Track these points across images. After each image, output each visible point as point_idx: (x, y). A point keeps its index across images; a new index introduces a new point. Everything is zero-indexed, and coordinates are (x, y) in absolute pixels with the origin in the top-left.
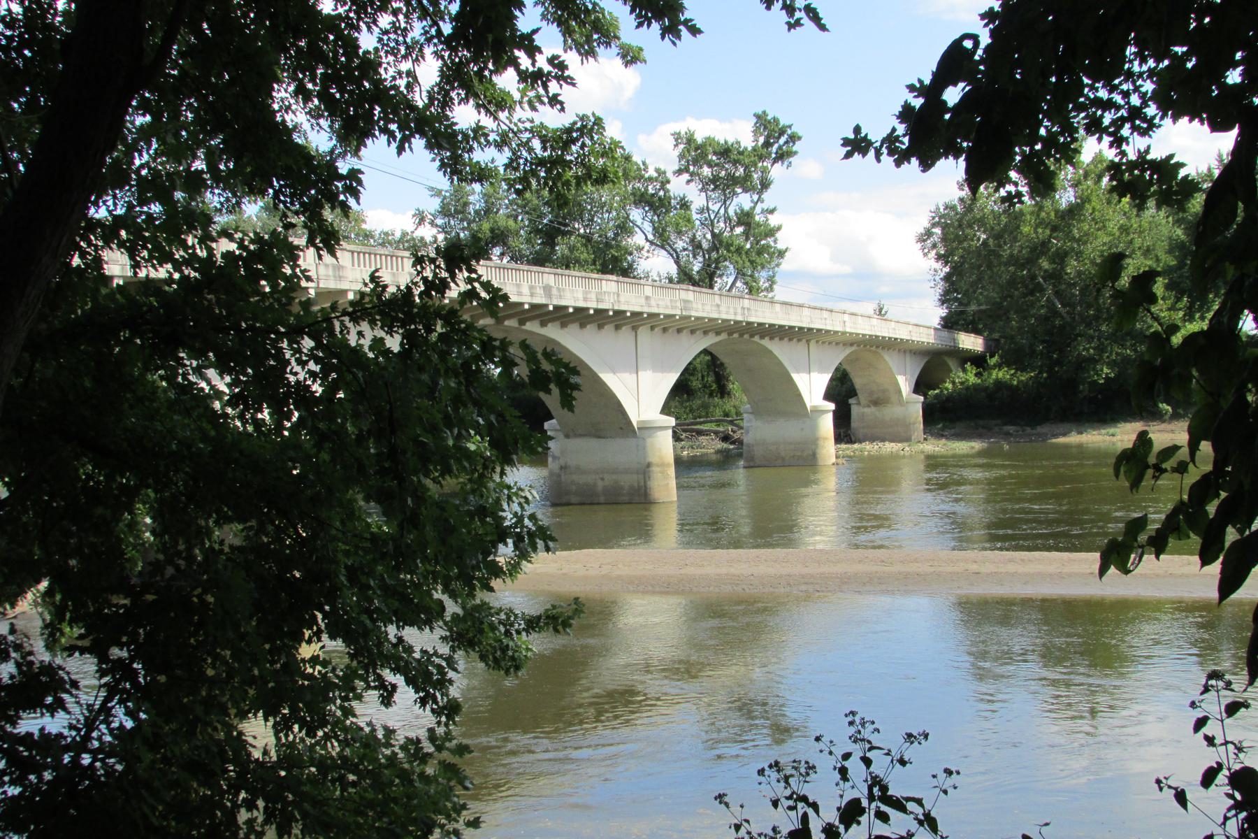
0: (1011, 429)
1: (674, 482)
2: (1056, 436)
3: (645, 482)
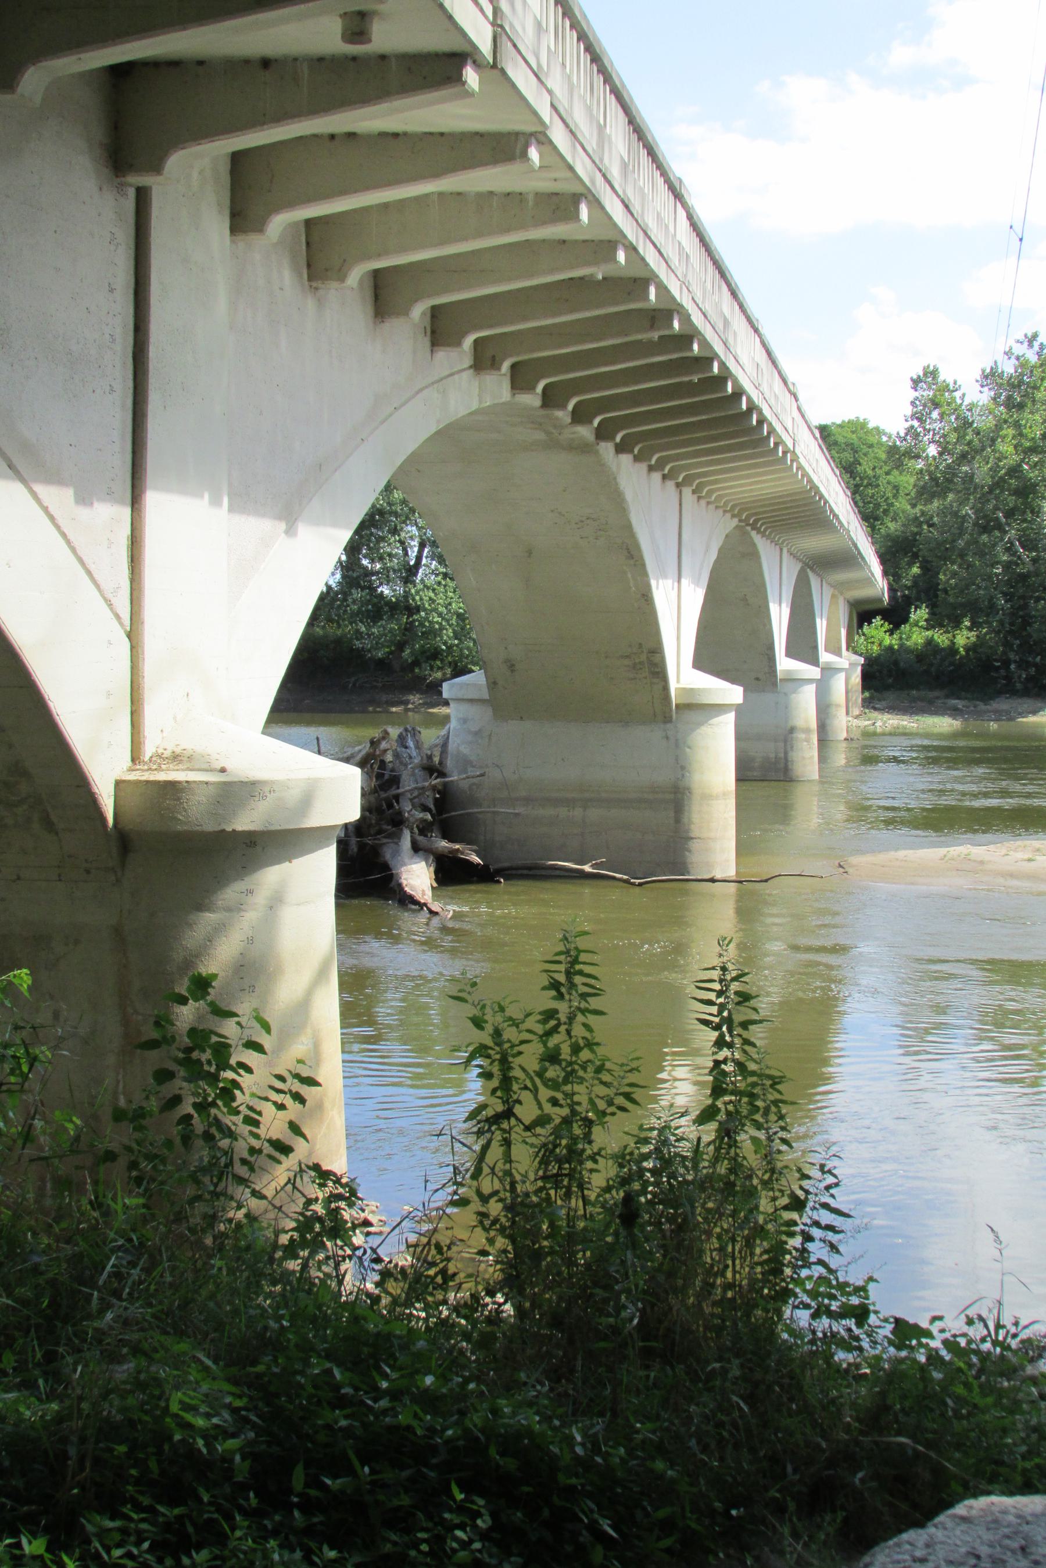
0: (959, 704)
1: (817, 767)
2: (1021, 714)
3: (786, 753)
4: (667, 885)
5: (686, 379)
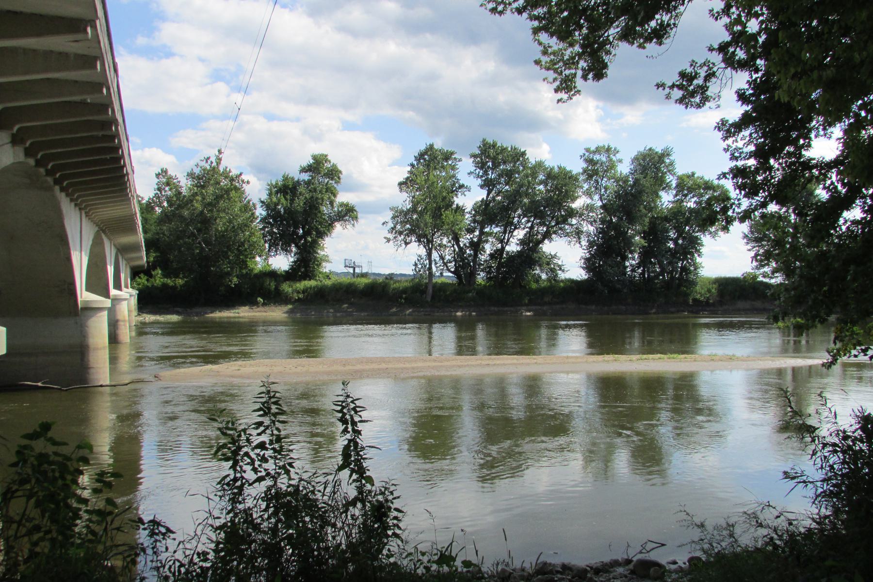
0: (180, 310)
2: (206, 313)
3: (115, 331)
4: (79, 390)
5: (103, 157)
